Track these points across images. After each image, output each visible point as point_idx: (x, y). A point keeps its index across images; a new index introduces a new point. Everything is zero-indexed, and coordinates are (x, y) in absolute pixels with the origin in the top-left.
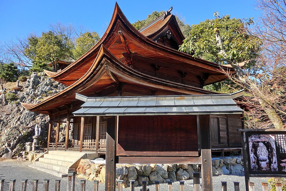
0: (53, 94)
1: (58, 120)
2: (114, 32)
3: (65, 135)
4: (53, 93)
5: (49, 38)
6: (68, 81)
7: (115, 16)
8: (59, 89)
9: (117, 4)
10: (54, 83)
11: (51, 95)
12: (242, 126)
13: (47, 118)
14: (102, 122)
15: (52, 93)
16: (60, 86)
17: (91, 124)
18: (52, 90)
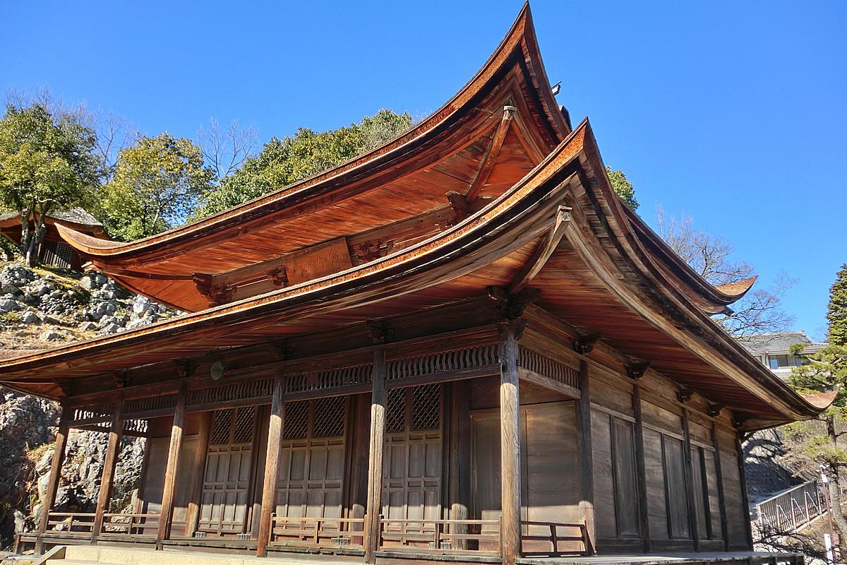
0: (22, 325)
1: (117, 418)
2: (482, 107)
3: (70, 482)
4: (24, 322)
5: (32, 127)
6: (154, 277)
7: (508, 50)
8: (46, 310)
9: (527, 8)
10: (27, 288)
11: (13, 328)
12: (741, 479)
13: (4, 414)
14: (232, 445)
15: (19, 321)
16: (49, 299)
17: (251, 444)
18: (18, 309)
